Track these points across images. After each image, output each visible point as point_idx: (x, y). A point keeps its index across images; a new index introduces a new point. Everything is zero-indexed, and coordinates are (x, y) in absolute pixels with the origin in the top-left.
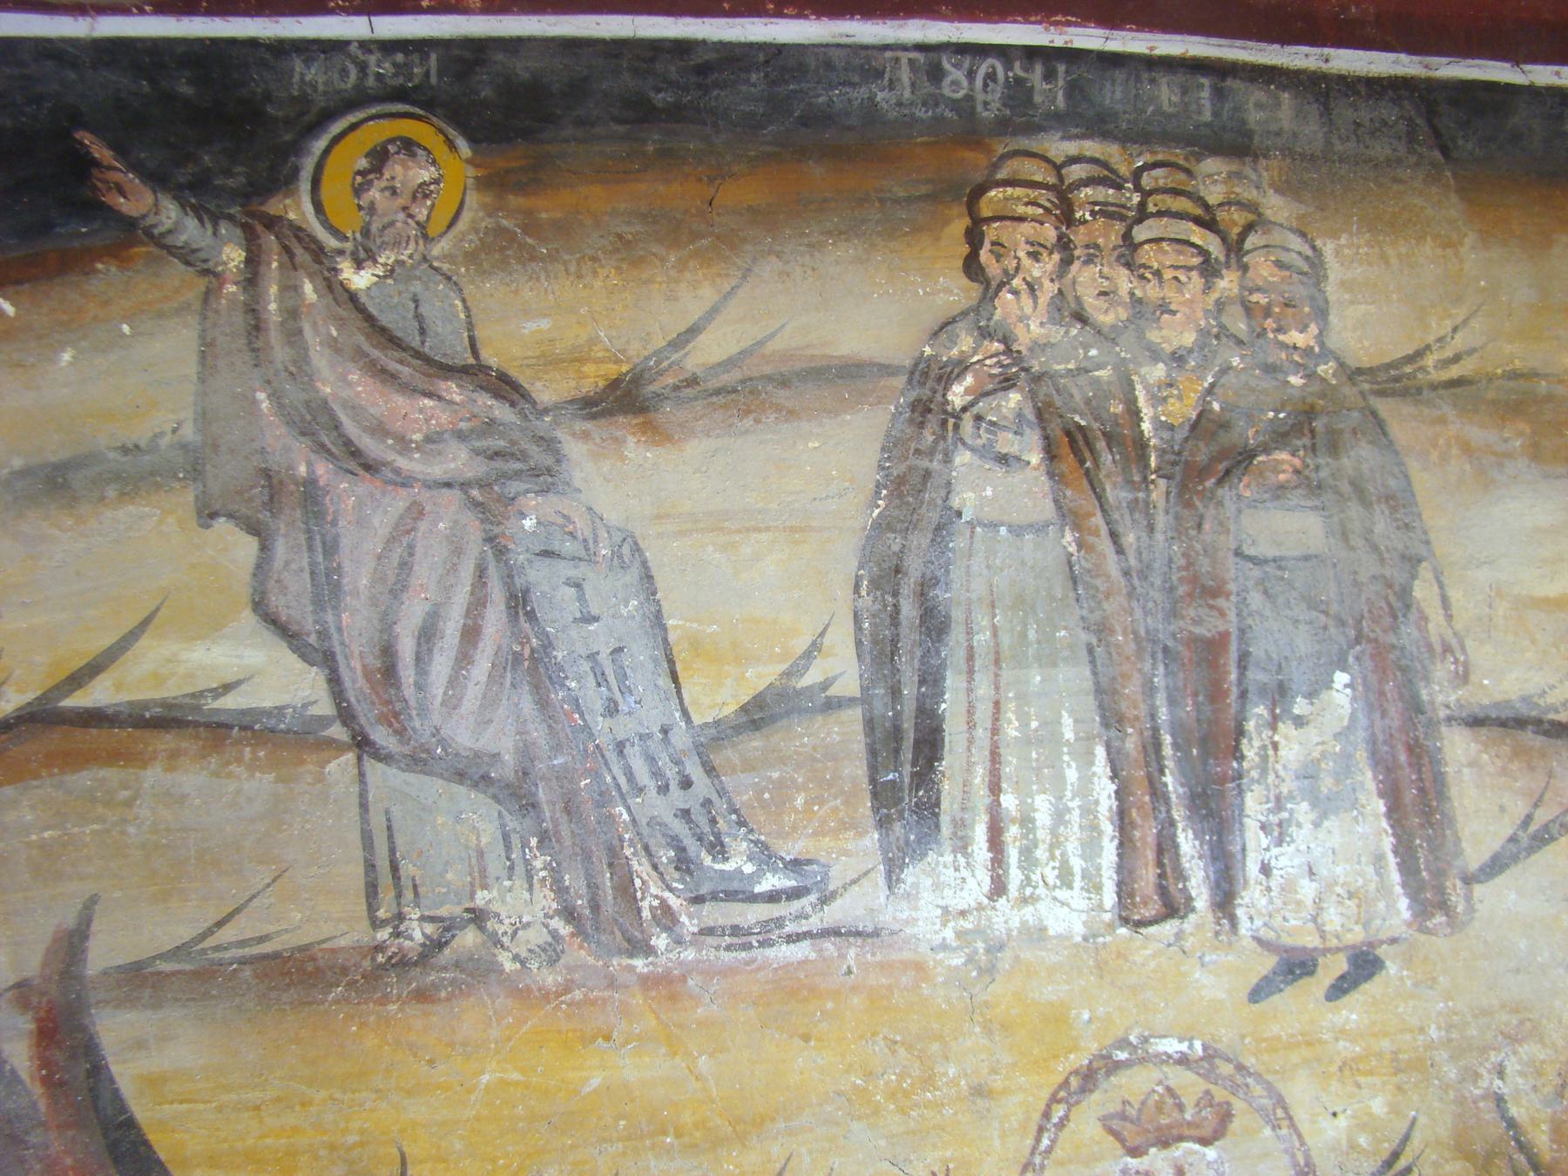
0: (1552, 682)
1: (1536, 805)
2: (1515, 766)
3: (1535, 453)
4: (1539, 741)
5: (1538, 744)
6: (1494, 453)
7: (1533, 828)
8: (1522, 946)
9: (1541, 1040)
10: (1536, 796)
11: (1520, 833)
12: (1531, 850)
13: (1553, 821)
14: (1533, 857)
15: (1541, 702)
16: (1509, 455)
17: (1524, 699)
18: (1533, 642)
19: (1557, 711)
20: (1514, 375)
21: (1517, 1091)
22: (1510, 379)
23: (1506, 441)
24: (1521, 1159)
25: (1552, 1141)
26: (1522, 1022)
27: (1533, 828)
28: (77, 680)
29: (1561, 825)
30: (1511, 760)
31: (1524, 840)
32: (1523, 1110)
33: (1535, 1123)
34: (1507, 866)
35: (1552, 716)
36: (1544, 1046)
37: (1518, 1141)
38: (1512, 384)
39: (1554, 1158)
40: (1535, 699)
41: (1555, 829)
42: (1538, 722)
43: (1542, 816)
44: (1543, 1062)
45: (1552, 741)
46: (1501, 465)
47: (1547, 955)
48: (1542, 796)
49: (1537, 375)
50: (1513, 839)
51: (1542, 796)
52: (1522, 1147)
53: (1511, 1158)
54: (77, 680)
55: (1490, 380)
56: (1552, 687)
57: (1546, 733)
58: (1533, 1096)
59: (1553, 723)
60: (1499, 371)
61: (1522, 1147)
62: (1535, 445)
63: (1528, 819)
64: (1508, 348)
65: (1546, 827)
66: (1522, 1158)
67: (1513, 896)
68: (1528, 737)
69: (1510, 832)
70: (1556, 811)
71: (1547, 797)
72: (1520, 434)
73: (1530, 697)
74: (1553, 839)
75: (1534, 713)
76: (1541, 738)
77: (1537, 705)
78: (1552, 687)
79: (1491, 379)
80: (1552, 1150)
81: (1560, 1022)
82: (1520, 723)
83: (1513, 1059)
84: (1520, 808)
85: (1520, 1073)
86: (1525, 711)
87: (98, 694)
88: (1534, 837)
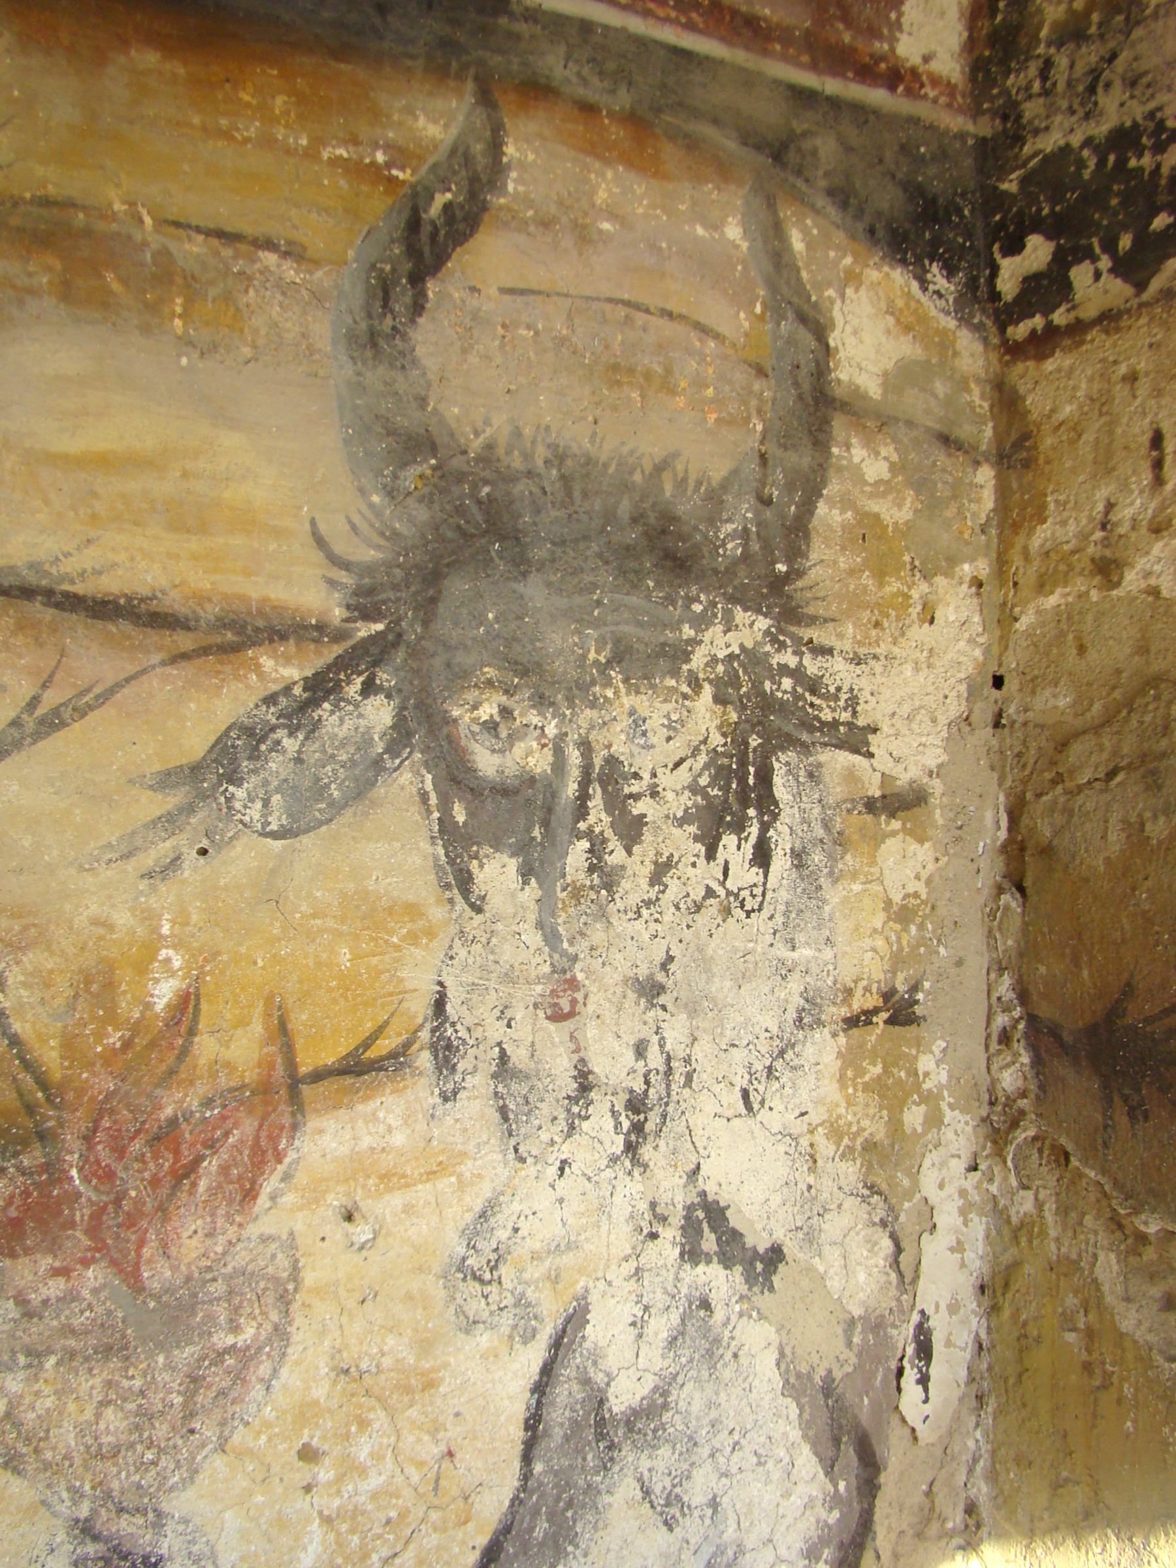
0: (66, 549)
1: (44, 686)
2: (20, 640)
3: (66, 292)
4: (50, 614)
5: (48, 618)
6: (14, 287)
7: (40, 711)
8: (27, 844)
9: (49, 947)
10: (45, 676)
11: (24, 716)
12: (37, 736)
13: (64, 704)
14: (40, 744)
15: (54, 571)
16: (32, 292)
17: (31, 566)
18: (47, 502)
19: (72, 582)
20: (46, 202)
21: (22, 1005)
22: (40, 205)
23: (30, 275)
24: (27, 1079)
25: (62, 1057)
26: (25, 928)
27: (40, 711)
28: (367, 1044)
29: (74, 709)
30: (14, 634)
31: (30, 723)
32: (28, 1026)
33: (43, 1039)
34: (8, 753)
35: (66, 587)
36: (52, 953)
37: (23, 1060)
38: (44, 212)
39: (65, 1077)
40: (46, 567)
41: (67, 714)
42: (49, 593)
43: (51, 699)
44: (51, 972)
45: (66, 615)
46: (21, 303)
47: (55, 853)
48: (51, 676)
49: (74, 205)
50: (15, 723)
51: (51, 676)
52: (27, 1065)
53: (15, 1079)
54: (367, 1044)
55: (15, 205)
56: (67, 555)
57: (58, 606)
58: (41, 1010)
59: (66, 595)
60: (28, 195)
61: (27, 1065)
62: (66, 284)
63: (34, 703)
64: (40, 171)
65: (56, 711)
66: (29, 1079)
67: (15, 788)
68: (37, 609)
69: (13, 714)
70: (69, 694)
71: (57, 677)
72: (49, 269)
73: (41, 564)
74: (64, 724)
75: (44, 582)
76: (51, 611)
77: (48, 574)
78: (67, 555)
79: (16, 202)
80: (63, 1068)
81: (71, 928)
82: (27, 592)
83: (15, 968)
84: (25, 689)
85: (24, 984)
86: (32, 579)
87: (371, 1054)
88: (42, 721)
